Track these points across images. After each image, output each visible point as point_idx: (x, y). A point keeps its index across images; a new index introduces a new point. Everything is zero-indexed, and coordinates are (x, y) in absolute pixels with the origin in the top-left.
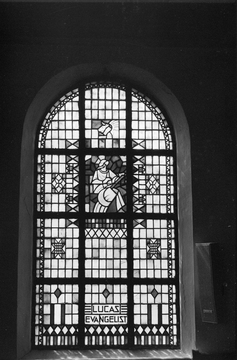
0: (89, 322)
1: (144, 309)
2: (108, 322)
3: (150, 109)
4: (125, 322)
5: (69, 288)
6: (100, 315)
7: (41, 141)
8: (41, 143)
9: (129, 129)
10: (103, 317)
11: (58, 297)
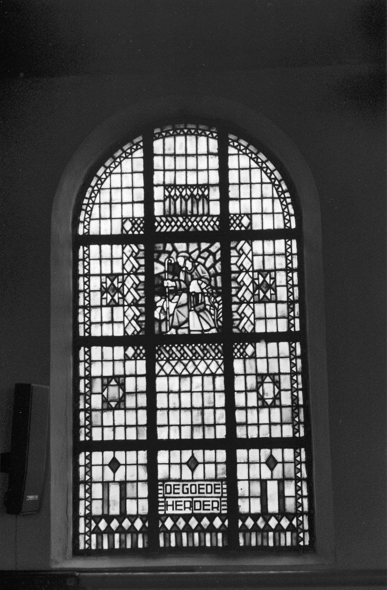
1: (256, 488)
3: (259, 165)
11: (272, 469)
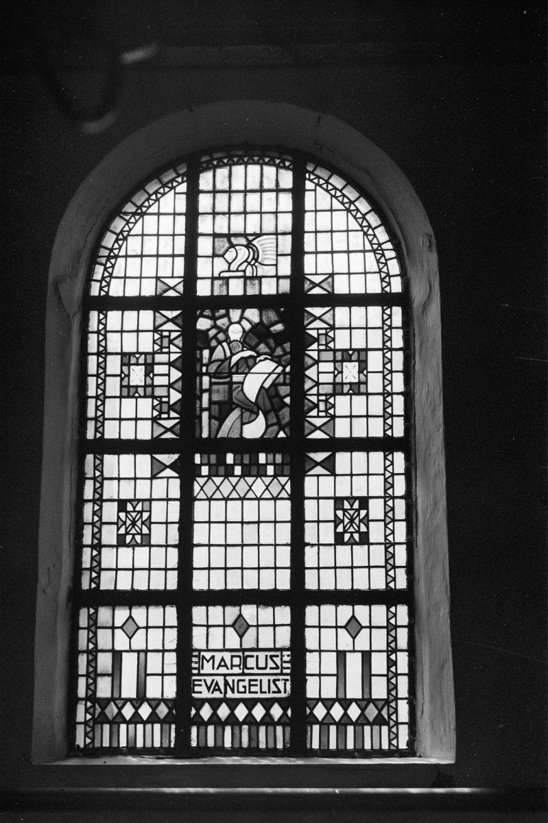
0: (201, 692)
2: (245, 692)
4: (285, 692)
5: (156, 614)
6: (225, 675)
7: (100, 282)
8: (385, 258)
9: (298, 254)
10: (233, 681)
